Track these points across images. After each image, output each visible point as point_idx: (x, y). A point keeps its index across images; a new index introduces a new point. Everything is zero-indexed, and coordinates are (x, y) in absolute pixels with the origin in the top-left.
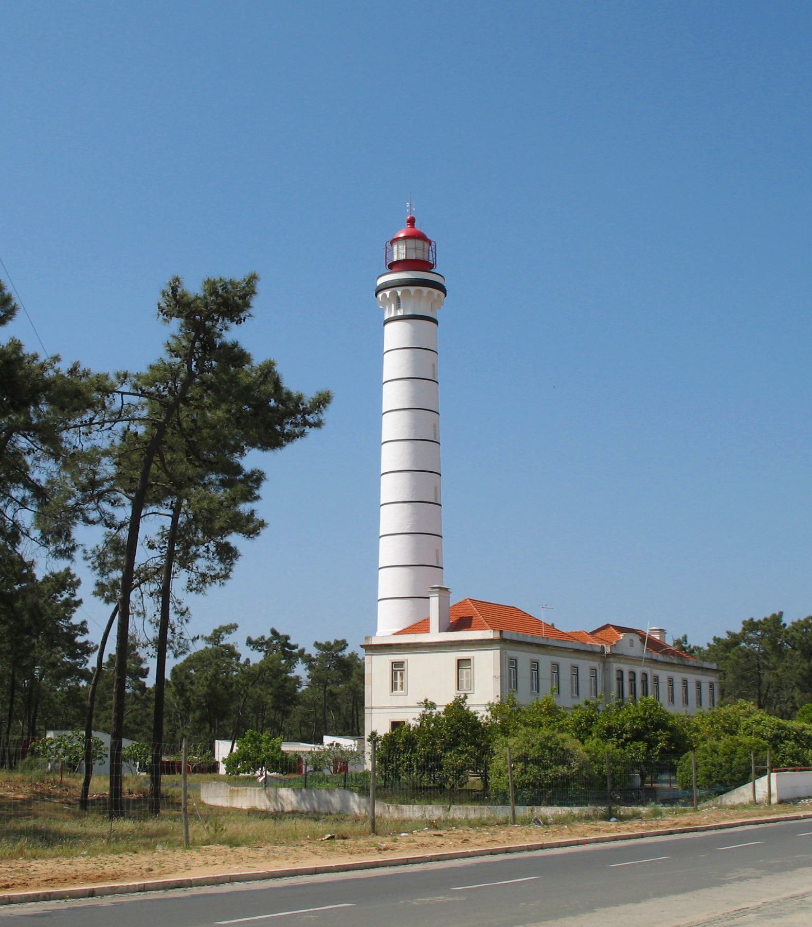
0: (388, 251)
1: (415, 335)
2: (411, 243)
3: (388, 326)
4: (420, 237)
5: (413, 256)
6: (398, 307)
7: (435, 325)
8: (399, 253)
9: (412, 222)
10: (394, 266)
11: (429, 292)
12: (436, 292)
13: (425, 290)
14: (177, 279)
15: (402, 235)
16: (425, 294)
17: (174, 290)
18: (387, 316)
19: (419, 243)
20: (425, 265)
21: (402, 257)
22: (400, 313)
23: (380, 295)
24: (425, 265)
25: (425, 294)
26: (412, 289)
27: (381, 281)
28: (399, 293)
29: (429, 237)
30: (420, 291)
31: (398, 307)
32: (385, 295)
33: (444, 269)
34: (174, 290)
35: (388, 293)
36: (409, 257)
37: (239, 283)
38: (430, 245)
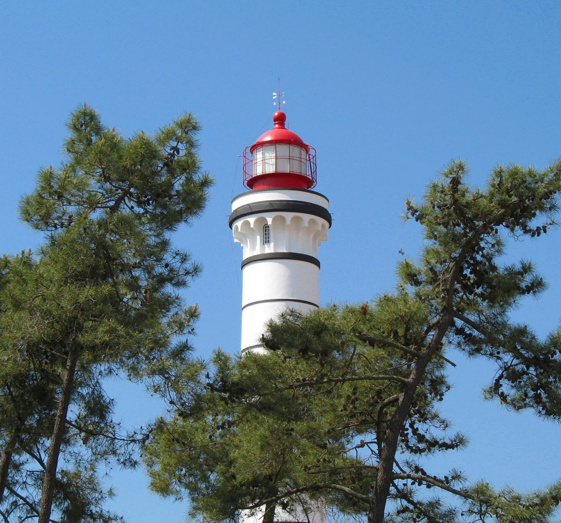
0: (248, 163)
1: (294, 281)
2: (284, 149)
3: (247, 270)
4: (293, 141)
5: (286, 168)
6: (266, 240)
7: (314, 267)
8: (265, 163)
9: (280, 119)
10: (255, 183)
11: (312, 222)
12: (320, 221)
13: (306, 217)
14: (461, 167)
15: (268, 139)
16: (306, 223)
17: (456, 182)
18: (247, 254)
19: (296, 151)
20: (300, 182)
21: (271, 169)
22: (269, 249)
23: (239, 224)
24: (300, 182)
25: (288, 222)
26: (289, 216)
27: (237, 204)
28: (270, 221)
29: (305, 142)
30: (283, 219)
31: (266, 240)
32: (247, 223)
33: (328, 188)
34: (456, 182)
35: (252, 220)
36: (280, 170)
37: (545, 175)
38: (307, 151)
